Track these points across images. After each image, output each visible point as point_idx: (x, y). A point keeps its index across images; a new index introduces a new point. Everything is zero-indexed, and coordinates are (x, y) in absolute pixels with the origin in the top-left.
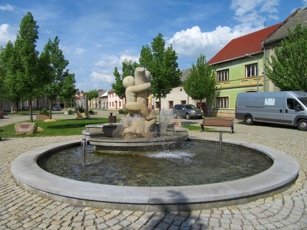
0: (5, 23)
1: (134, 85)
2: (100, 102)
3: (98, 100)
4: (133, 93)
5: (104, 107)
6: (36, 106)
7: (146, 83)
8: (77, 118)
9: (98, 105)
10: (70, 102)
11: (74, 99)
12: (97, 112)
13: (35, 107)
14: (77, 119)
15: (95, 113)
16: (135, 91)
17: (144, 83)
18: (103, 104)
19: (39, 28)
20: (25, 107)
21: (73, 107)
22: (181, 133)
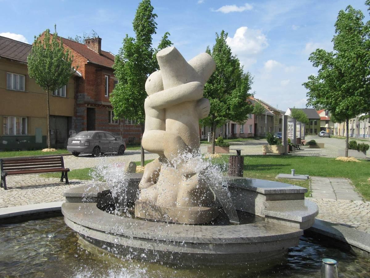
0: (241, 27)
1: (162, 89)
2: (358, 126)
3: (355, 122)
4: (154, 110)
5: (364, 135)
6: (253, 132)
7: (185, 83)
8: (266, 153)
9: (355, 130)
10: (311, 126)
11: (318, 122)
12: (323, 144)
13: (251, 133)
14: (265, 156)
15: (318, 145)
16: (154, 106)
17: (179, 84)
18: (362, 129)
19: (157, 17)
20: (236, 134)
21: (317, 134)
22: (283, 223)
